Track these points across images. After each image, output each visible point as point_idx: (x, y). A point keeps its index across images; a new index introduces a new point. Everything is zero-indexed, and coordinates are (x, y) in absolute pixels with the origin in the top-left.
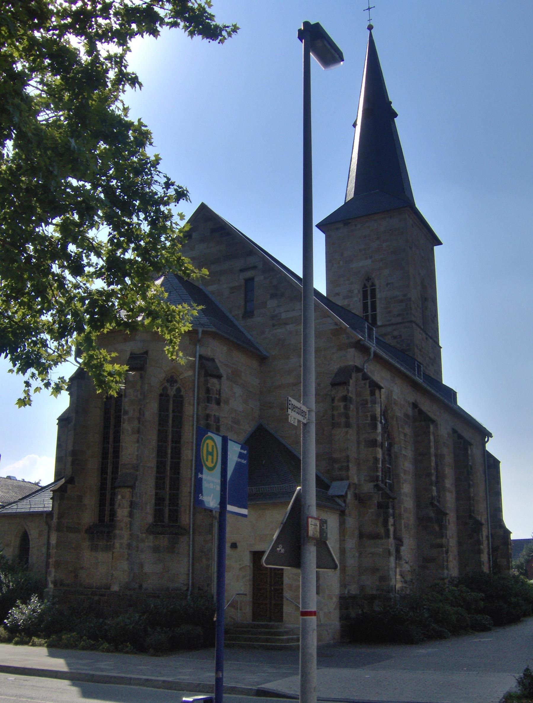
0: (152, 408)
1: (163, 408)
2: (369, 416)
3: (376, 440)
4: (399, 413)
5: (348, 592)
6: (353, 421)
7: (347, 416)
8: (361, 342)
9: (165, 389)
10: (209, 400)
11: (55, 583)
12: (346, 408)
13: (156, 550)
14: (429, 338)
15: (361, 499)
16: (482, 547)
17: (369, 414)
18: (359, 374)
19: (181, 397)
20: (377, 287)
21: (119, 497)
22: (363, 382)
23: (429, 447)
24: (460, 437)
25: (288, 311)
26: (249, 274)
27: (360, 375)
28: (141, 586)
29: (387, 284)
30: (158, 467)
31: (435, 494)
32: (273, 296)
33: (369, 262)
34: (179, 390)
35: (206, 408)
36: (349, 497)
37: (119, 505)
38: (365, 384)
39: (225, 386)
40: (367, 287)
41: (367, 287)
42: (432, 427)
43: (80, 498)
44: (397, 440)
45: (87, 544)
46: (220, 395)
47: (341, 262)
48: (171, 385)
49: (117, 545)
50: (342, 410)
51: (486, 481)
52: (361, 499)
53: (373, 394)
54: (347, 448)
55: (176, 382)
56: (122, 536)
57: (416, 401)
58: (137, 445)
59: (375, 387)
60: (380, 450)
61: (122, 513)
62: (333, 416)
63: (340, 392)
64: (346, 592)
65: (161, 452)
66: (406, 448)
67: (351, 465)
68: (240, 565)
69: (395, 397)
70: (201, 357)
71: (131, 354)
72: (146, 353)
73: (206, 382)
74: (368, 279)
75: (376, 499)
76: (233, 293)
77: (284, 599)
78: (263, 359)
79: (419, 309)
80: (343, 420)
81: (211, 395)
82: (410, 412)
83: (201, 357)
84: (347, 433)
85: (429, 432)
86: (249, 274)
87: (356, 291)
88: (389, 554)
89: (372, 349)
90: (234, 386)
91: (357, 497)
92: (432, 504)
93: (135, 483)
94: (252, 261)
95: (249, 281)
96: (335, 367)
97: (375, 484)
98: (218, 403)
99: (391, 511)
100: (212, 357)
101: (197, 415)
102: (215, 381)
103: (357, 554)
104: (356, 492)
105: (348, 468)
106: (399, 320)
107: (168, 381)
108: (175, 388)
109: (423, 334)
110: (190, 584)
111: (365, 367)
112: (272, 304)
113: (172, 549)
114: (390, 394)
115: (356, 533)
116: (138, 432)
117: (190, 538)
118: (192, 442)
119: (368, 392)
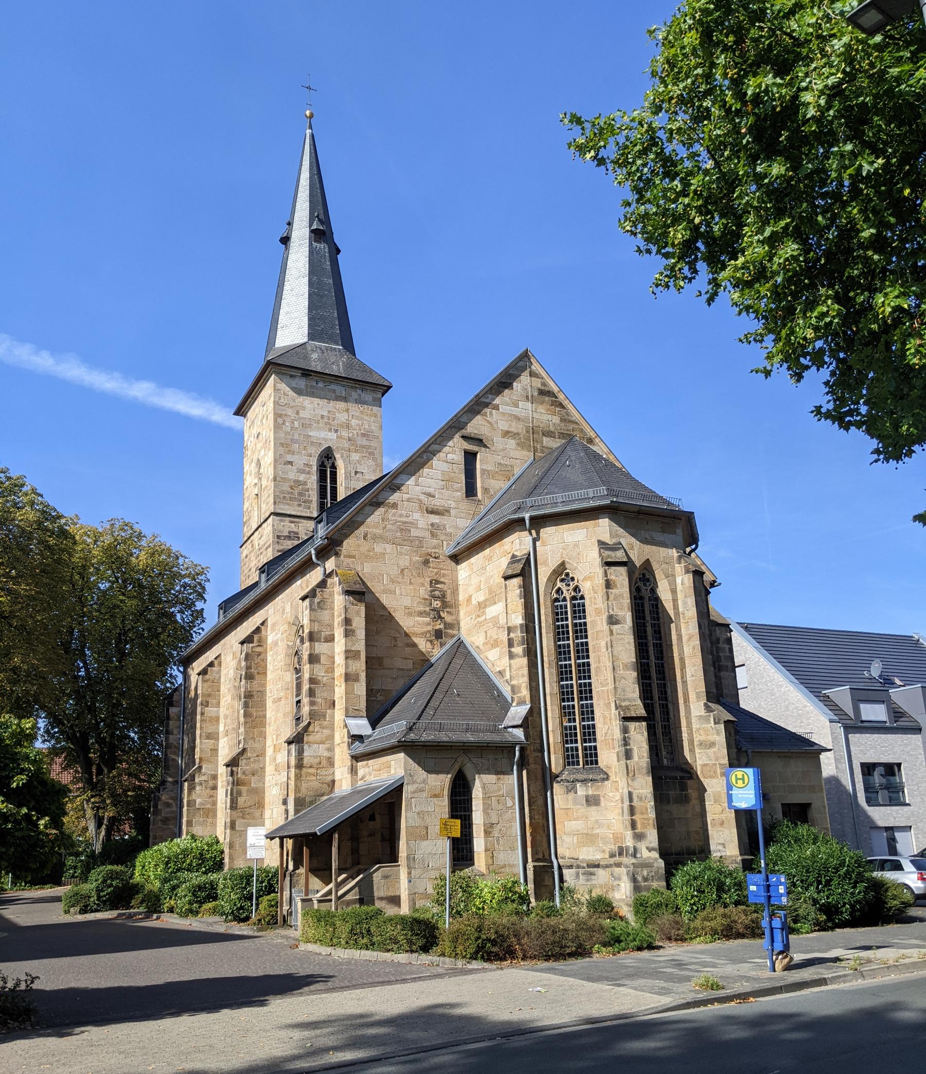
29: (356, 473)
33: (333, 436)
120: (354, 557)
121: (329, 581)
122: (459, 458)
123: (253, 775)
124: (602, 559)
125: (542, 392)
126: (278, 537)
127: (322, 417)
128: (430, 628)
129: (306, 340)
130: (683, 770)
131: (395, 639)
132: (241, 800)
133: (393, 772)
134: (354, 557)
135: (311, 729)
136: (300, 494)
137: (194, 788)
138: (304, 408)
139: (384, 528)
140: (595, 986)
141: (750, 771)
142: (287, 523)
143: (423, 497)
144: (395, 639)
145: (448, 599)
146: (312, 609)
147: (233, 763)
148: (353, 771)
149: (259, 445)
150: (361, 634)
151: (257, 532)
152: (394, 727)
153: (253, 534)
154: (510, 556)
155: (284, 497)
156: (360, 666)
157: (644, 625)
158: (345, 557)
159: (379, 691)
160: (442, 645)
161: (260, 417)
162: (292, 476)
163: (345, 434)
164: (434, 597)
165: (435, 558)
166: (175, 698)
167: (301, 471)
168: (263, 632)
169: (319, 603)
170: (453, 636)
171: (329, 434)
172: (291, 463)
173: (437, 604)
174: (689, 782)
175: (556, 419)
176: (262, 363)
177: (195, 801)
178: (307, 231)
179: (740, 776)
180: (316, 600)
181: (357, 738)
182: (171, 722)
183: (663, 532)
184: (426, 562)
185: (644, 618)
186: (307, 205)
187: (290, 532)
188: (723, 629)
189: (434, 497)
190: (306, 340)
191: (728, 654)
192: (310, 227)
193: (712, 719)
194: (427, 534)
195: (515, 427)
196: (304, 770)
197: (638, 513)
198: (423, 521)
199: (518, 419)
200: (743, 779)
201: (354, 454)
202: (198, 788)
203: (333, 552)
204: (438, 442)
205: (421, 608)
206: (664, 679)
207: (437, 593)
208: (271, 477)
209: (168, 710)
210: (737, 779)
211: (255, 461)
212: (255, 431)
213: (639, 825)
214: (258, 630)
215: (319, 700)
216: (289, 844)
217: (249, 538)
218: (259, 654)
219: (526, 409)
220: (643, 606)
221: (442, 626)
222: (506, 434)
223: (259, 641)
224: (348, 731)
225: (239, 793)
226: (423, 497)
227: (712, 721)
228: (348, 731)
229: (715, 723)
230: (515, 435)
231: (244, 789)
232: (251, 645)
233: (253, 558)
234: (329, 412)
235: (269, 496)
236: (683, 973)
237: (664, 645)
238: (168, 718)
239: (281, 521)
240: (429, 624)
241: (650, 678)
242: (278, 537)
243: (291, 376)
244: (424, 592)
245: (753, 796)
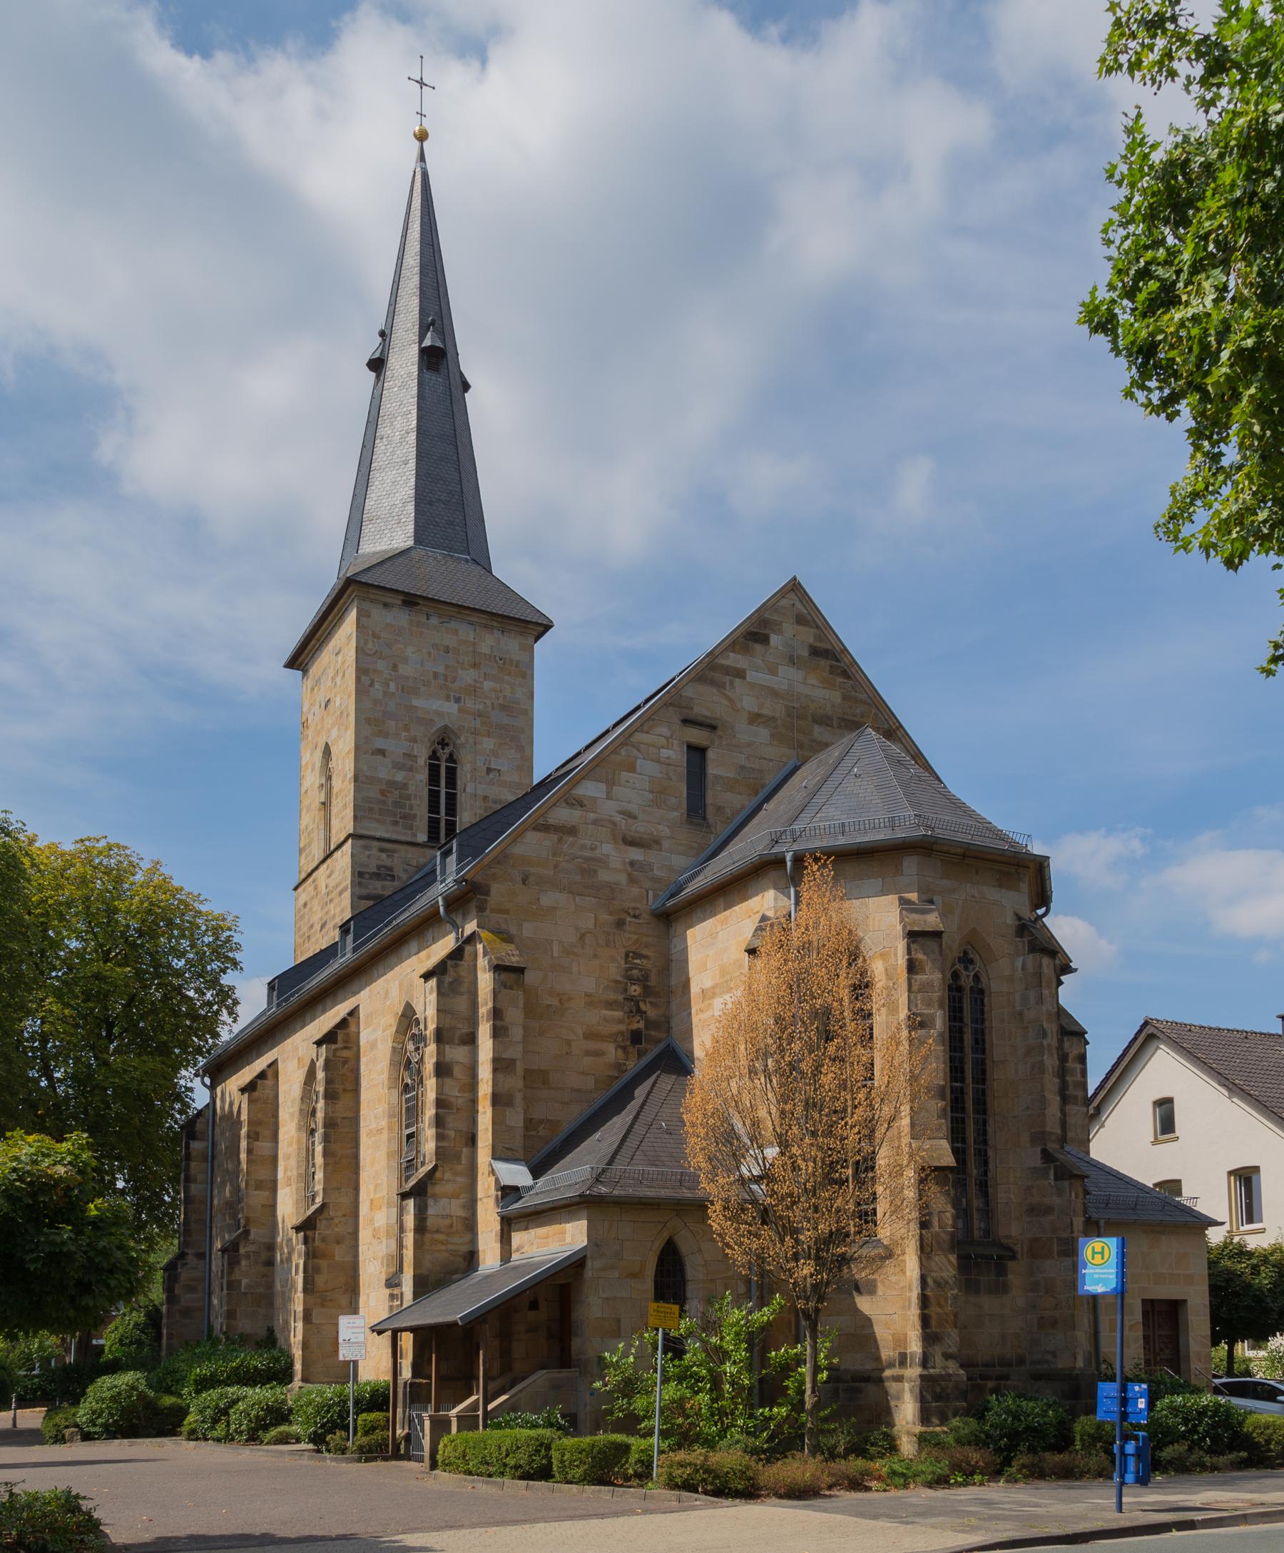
29: (489, 770)
33: (452, 708)
47: (392, 685)
120: (507, 912)
121: (468, 949)
122: (676, 754)
123: (338, 1243)
124: (904, 927)
125: (815, 652)
126: (361, 874)
127: (436, 675)
128: (622, 1027)
129: (410, 543)
130: (1002, 1246)
131: (569, 1043)
132: (320, 1280)
133: (568, 1240)
134: (507, 912)
135: (438, 1174)
136: (397, 804)
137: (238, 1262)
138: (405, 660)
139: (556, 867)
140: (873, 1523)
141: (1115, 1239)
142: (374, 852)
143: (618, 818)
144: (569, 1043)
145: (653, 982)
146: (440, 993)
147: (306, 1227)
148: (505, 1239)
149: (329, 721)
150: (517, 1033)
151: (325, 865)
152: (572, 1175)
153: (316, 868)
154: (758, 917)
155: (371, 809)
156: (514, 1082)
157: (961, 1031)
158: (493, 911)
159: (541, 1121)
160: (641, 1054)
161: (331, 672)
162: (384, 773)
163: (469, 703)
164: (630, 978)
165: (635, 916)
166: (199, 1126)
167: (398, 766)
168: (353, 1028)
169: (451, 983)
170: (659, 1041)
171: (447, 704)
172: (382, 752)
173: (635, 990)
174: (1011, 1264)
175: (836, 696)
176: (329, 581)
177: (239, 1282)
178: (414, 351)
179: (1098, 1249)
180: (448, 979)
181: (508, 1193)
182: (193, 1164)
183: (1000, 886)
184: (620, 924)
185: (961, 1020)
186: (415, 302)
187: (379, 867)
188: (1075, 1039)
189: (635, 818)
190: (410, 543)
191: (1079, 1078)
192: (421, 342)
193: (1052, 1173)
194: (623, 879)
195: (771, 708)
196: (428, 1235)
197: (964, 856)
198: (615, 856)
199: (774, 693)
200: (1102, 1253)
201: (486, 740)
202: (244, 1263)
203: (474, 904)
204: (645, 728)
205: (612, 996)
206: (985, 1112)
207: (635, 972)
208: (351, 775)
209: (187, 1147)
210: (1094, 1253)
211: (321, 747)
212: (321, 697)
213: (933, 1323)
214: (343, 1024)
215: (452, 1134)
216: (407, 1340)
217: (310, 875)
218: (345, 1061)
219: (788, 678)
220: (960, 999)
221: (641, 1025)
222: (755, 718)
223: (346, 1041)
224: (497, 1180)
225: (317, 1270)
226: (618, 818)
227: (1052, 1177)
228: (497, 1180)
229: (1056, 1179)
230: (767, 721)
231: (323, 1263)
232: (334, 1047)
233: (316, 908)
234: (447, 667)
235: (345, 806)
236: (994, 1512)
237: (988, 1061)
238: (188, 1157)
239: (366, 848)
240: (620, 1021)
241: (963, 1110)
242: (361, 874)
243: (386, 605)
244: (614, 971)
245: (1113, 1277)
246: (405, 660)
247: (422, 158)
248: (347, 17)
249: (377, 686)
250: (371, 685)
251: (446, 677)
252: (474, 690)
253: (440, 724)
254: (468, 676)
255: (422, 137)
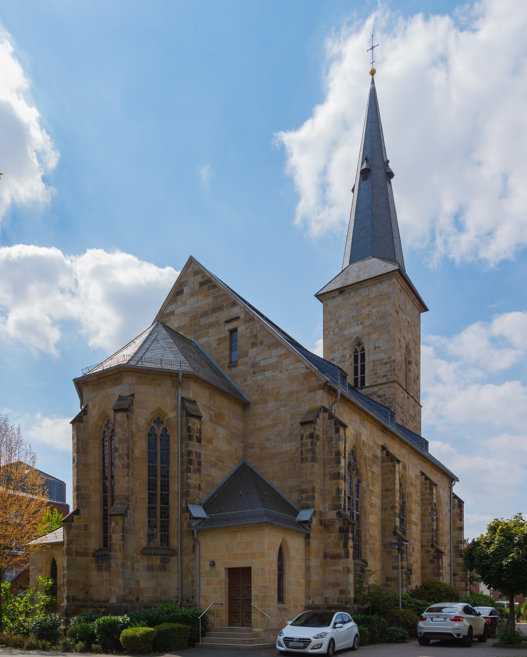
0: (141, 446)
1: (151, 446)
2: (334, 451)
3: (339, 473)
4: (368, 454)
5: (313, 602)
6: (318, 456)
7: (313, 451)
8: (328, 384)
9: (152, 429)
10: (190, 438)
11: (68, 598)
12: (312, 444)
13: (150, 568)
14: (410, 397)
15: (325, 525)
16: (441, 570)
17: (333, 450)
18: (326, 414)
19: (168, 436)
20: (366, 352)
21: (113, 524)
22: (329, 421)
23: (394, 484)
24: (427, 478)
25: (266, 358)
26: (232, 326)
27: (326, 415)
28: (138, 599)
29: (375, 348)
30: (149, 498)
31: (398, 523)
32: (254, 345)
33: (359, 328)
34: (165, 430)
35: (187, 446)
36: (314, 522)
37: (113, 531)
38: (331, 423)
39: (208, 428)
40: (358, 352)
41: (358, 352)
42: (397, 466)
43: (86, 527)
44: (364, 477)
45: (93, 565)
46: (200, 434)
47: (336, 330)
48: (157, 426)
49: (113, 565)
50: (309, 447)
51: (451, 518)
52: (325, 525)
53: (337, 431)
54: (313, 480)
55: (162, 422)
56: (117, 558)
57: (385, 445)
58: (127, 478)
59: (340, 425)
60: (342, 482)
61: (116, 538)
62: (302, 451)
63: (309, 430)
64: (311, 603)
65: (152, 486)
66: (373, 485)
67: (316, 496)
68: (217, 579)
69: (363, 438)
70: (183, 399)
71: (120, 396)
72: (133, 395)
73: (187, 422)
74: (359, 344)
75: (338, 525)
76: (220, 344)
77: (252, 609)
78: (245, 405)
79: (402, 371)
80: (310, 455)
81: (192, 434)
82: (379, 453)
83: (183, 399)
84: (313, 466)
85: (395, 470)
86: (232, 326)
87: (348, 356)
88: (348, 571)
89: (339, 391)
90: (218, 427)
91: (322, 523)
92: (395, 533)
93: (126, 511)
94: (236, 311)
95: (233, 331)
96: (305, 408)
97: (337, 511)
98: (199, 440)
99: (351, 535)
100: (194, 399)
101: (181, 451)
102: (196, 420)
103: (321, 572)
104: (322, 518)
105: (313, 498)
106: (384, 380)
107: (155, 421)
108: (161, 428)
109: (405, 393)
110: (180, 597)
111: (333, 408)
112: (252, 352)
113: (163, 567)
114: (357, 436)
115: (322, 554)
116: (128, 467)
117: (178, 558)
118: (178, 476)
119: (334, 430)
171: (357, 327)
243: (333, 298)
246: (341, 317)
247: (373, 82)
248: (438, 17)
249: (331, 333)
250: (329, 334)
251: (357, 315)
252: (368, 316)
253: (355, 337)
254: (365, 311)
255: (373, 73)
